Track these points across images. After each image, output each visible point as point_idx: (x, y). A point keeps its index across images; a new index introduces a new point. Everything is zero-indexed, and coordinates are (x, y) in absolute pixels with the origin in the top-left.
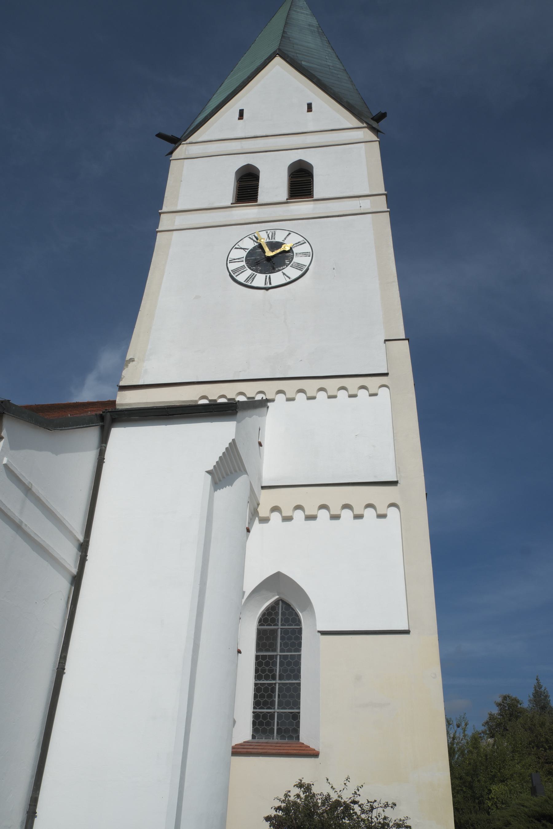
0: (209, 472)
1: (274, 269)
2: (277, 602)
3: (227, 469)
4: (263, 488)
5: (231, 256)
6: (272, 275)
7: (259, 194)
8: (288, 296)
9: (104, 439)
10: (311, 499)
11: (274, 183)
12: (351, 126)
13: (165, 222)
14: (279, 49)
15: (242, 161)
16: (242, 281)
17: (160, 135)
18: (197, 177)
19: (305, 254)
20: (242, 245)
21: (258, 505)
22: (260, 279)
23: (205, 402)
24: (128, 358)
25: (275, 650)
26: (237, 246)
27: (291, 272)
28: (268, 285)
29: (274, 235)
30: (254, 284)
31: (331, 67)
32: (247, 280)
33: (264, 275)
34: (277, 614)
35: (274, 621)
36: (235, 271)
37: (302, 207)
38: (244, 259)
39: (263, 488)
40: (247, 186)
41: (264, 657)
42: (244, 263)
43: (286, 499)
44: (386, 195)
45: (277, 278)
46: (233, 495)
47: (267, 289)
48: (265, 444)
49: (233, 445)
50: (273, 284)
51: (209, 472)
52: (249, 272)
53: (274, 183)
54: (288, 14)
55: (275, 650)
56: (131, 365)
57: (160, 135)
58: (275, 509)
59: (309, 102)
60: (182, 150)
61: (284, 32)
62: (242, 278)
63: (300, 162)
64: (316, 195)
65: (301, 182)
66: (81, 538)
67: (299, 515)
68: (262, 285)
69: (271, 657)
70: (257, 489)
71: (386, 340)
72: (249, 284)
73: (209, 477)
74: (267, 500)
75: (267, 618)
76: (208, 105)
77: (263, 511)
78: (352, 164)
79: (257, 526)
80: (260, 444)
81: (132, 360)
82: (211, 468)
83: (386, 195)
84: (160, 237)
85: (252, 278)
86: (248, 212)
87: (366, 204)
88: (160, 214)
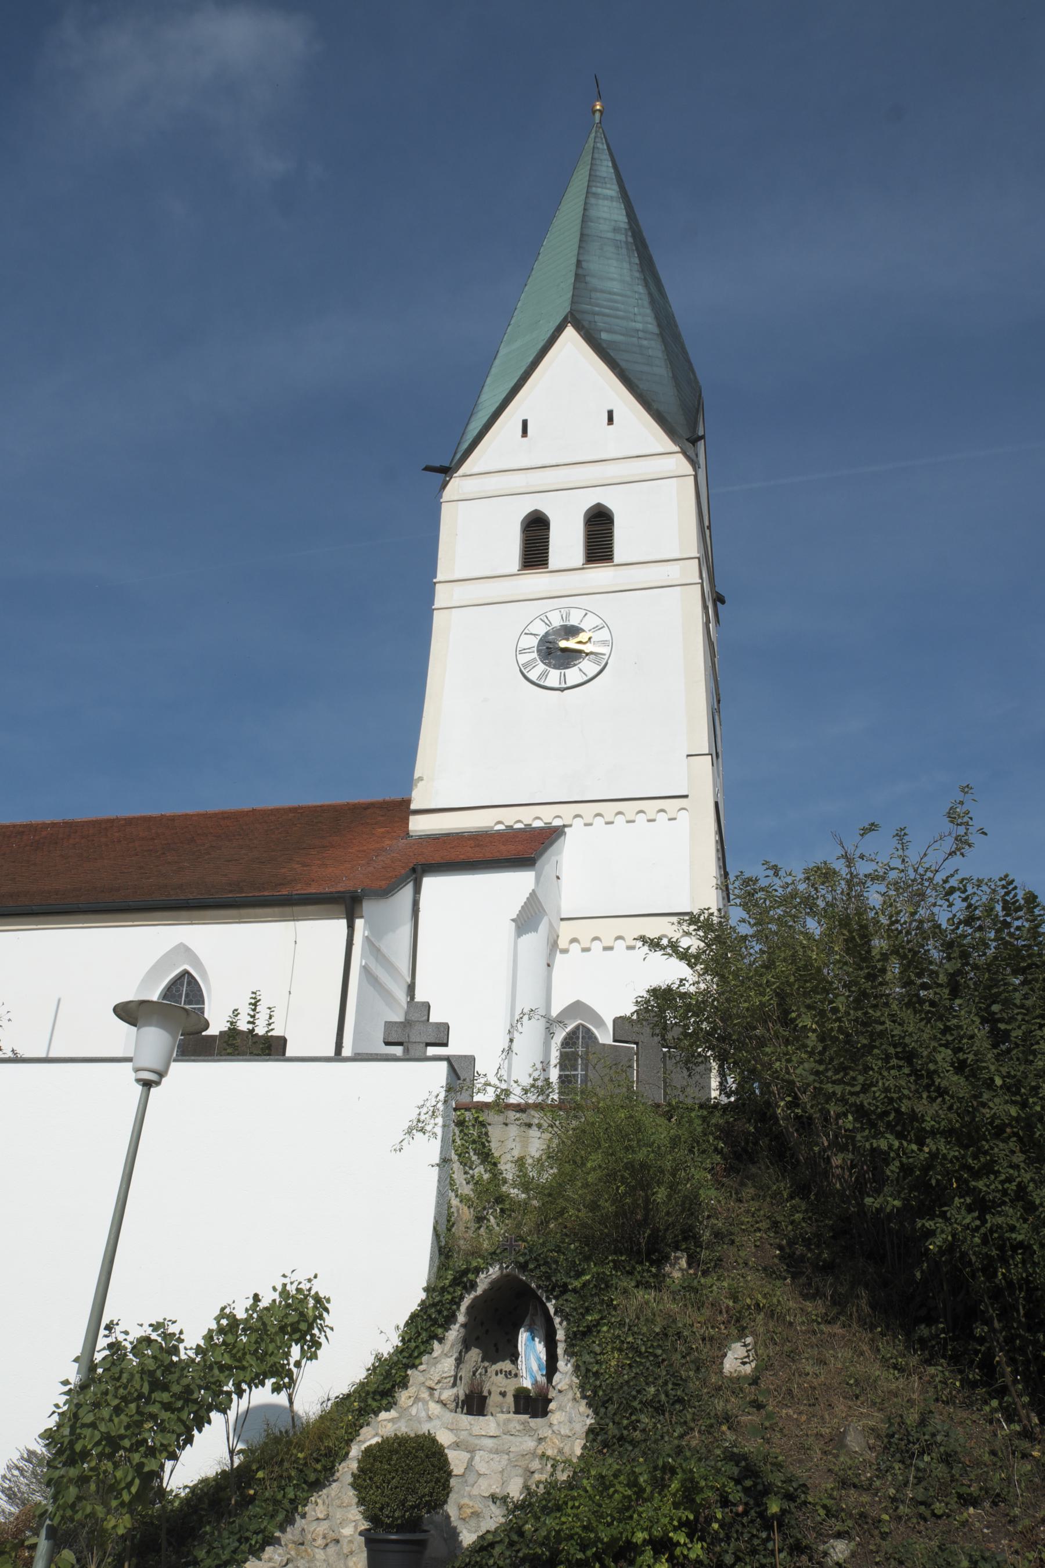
0: (513, 920)
1: (568, 663)
2: (577, 1027)
3: (528, 919)
4: (562, 919)
5: (521, 646)
6: (567, 671)
7: (550, 554)
8: (584, 703)
9: (417, 890)
10: (608, 930)
11: (567, 540)
12: (662, 450)
13: (442, 596)
14: (571, 313)
15: (525, 507)
16: (534, 679)
17: (428, 469)
18: (473, 526)
19: (604, 643)
20: (532, 629)
21: (558, 937)
22: (554, 677)
23: (501, 827)
24: (416, 776)
25: (576, 1070)
26: (526, 631)
27: (588, 667)
28: (563, 686)
29: (568, 615)
30: (547, 684)
31: (641, 334)
32: (539, 678)
33: (558, 672)
34: (578, 1038)
35: (575, 1044)
36: (526, 665)
37: (601, 575)
38: (535, 649)
39: (562, 919)
40: (536, 532)
41: (567, 1076)
42: (535, 655)
43: (584, 930)
44: (699, 558)
45: (573, 675)
46: (533, 942)
47: (562, 690)
48: (563, 878)
49: (533, 895)
50: (569, 684)
51: (513, 920)
52: (541, 667)
53: (567, 540)
54: (585, 209)
55: (576, 1070)
56: (420, 784)
57: (428, 469)
58: (574, 940)
59: (610, 408)
60: (456, 487)
61: (579, 263)
62: (533, 675)
63: (599, 506)
64: (617, 559)
65: (599, 528)
66: (409, 980)
67: (597, 946)
68: (557, 685)
69: (574, 1075)
70: (555, 921)
71: (688, 756)
72: (541, 683)
73: (513, 924)
74: (566, 932)
75: (570, 1041)
76: (482, 399)
77: (563, 943)
78: (660, 503)
79: (559, 956)
80: (558, 878)
81: (421, 779)
82: (515, 917)
83: (699, 558)
84: (437, 616)
85: (544, 675)
86: (536, 581)
87: (673, 572)
88: (435, 583)
